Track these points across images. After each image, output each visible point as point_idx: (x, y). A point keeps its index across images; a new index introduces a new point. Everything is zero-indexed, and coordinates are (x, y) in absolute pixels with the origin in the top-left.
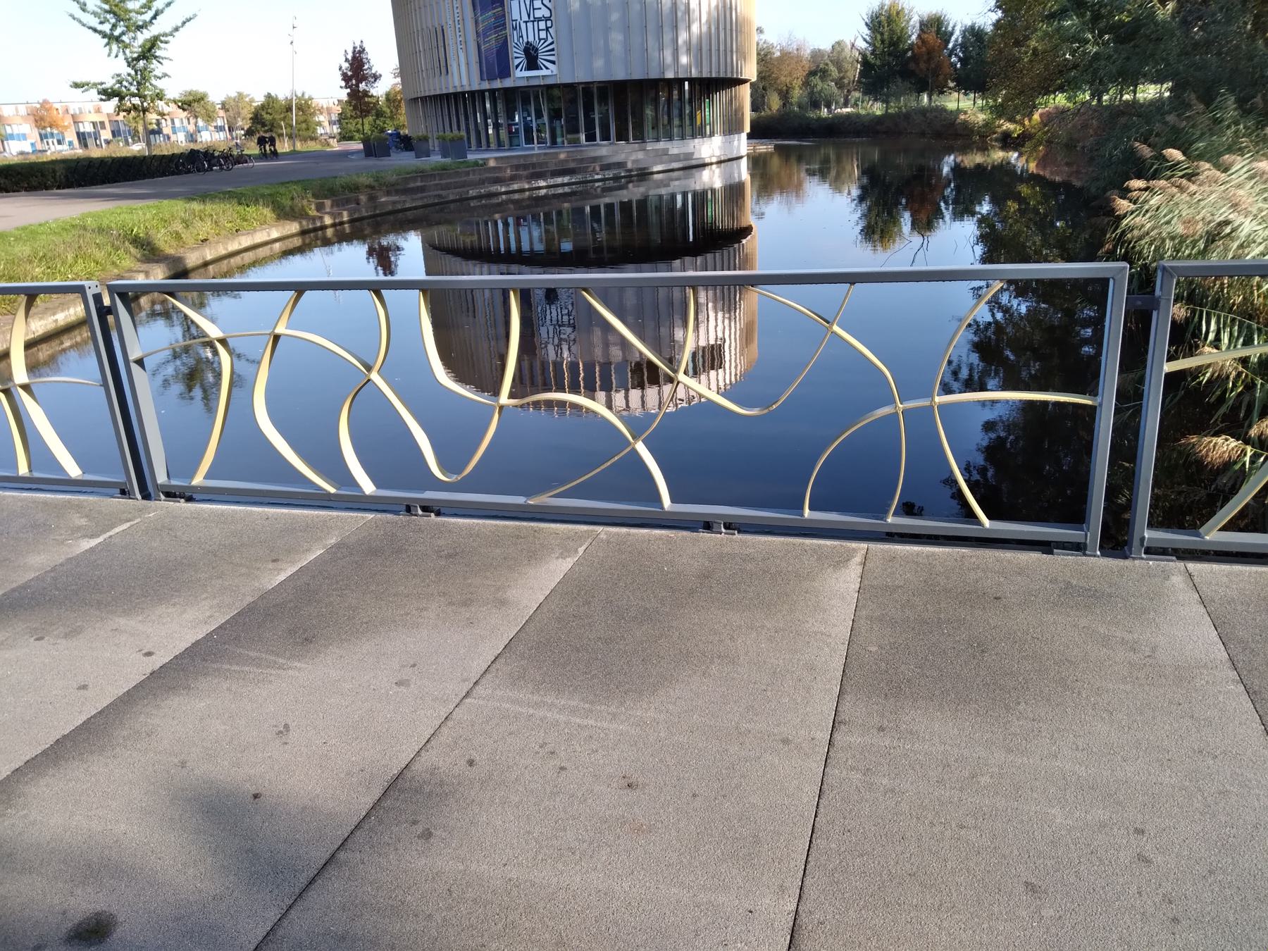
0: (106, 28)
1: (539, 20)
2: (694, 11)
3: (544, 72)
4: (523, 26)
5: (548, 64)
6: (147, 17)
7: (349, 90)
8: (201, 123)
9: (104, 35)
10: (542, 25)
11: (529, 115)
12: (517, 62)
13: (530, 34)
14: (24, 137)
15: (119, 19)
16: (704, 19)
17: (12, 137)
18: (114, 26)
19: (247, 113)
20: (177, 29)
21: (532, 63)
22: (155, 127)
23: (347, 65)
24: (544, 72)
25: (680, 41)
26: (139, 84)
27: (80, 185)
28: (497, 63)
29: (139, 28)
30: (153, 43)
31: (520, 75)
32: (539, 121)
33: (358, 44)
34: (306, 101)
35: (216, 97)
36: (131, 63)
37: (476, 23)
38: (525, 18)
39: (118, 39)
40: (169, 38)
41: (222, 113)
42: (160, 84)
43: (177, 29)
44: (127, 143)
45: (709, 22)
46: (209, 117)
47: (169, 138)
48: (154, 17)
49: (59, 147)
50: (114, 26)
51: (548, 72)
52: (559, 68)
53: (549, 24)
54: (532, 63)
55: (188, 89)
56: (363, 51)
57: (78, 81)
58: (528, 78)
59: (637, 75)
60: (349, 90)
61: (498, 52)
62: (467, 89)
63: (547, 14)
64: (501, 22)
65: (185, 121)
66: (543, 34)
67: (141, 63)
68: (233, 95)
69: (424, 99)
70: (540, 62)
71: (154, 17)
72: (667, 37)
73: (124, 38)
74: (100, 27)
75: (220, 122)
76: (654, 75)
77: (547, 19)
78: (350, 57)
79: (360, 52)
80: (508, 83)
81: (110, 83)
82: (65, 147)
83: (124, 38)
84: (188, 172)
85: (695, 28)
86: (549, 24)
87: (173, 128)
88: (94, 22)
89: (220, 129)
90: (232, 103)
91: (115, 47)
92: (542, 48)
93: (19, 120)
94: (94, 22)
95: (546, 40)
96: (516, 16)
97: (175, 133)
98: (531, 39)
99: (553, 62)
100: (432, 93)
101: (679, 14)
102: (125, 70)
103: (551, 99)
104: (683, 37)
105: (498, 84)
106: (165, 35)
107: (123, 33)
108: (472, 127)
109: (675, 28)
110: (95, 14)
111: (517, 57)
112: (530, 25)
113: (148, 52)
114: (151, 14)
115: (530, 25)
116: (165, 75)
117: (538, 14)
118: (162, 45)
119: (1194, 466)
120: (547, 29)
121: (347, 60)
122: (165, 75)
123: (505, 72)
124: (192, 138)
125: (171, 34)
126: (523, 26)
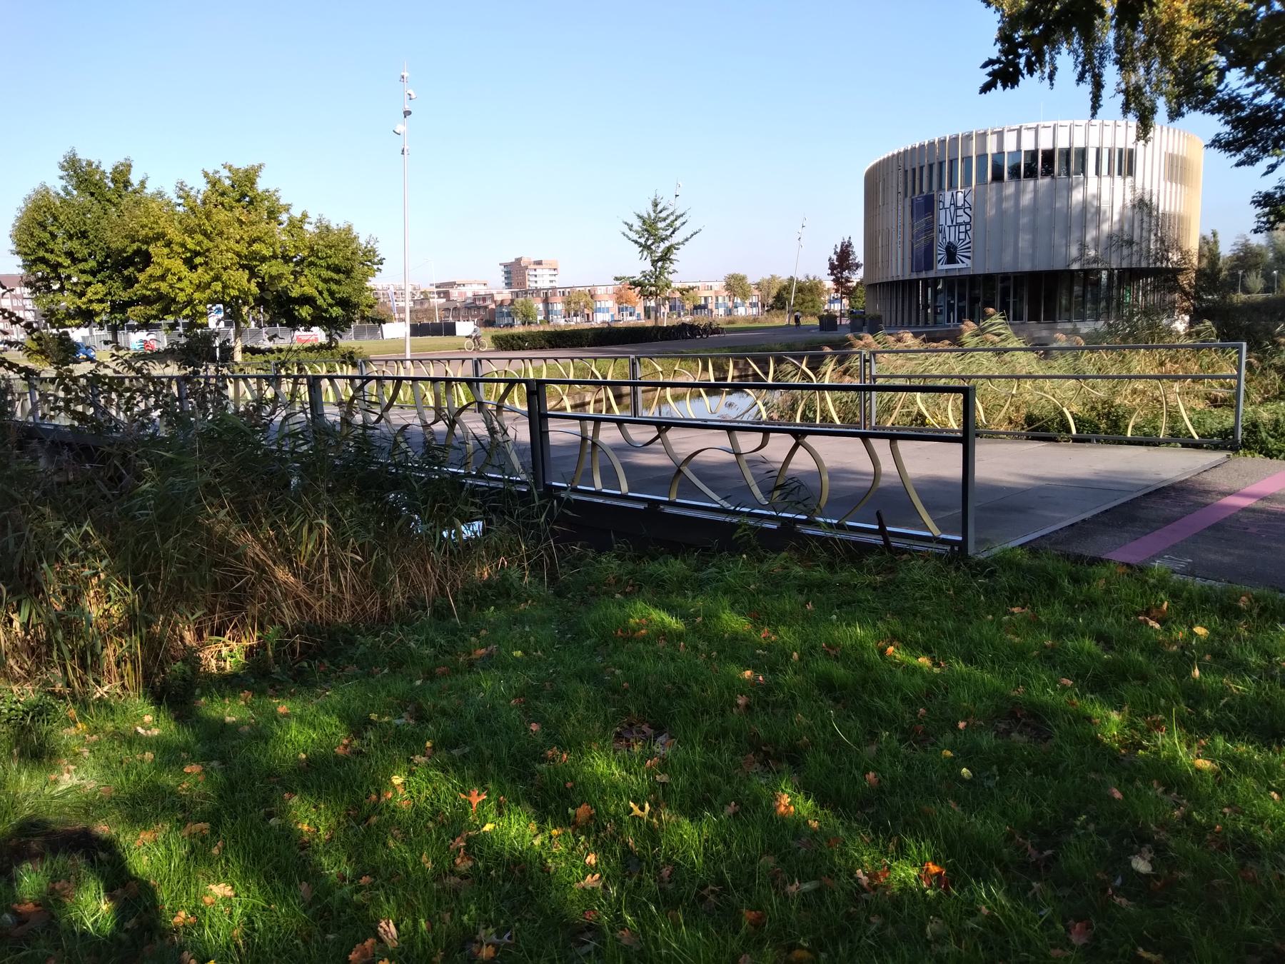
0: (642, 241)
1: (960, 224)
2: (1105, 212)
3: (960, 265)
4: (947, 229)
5: (963, 259)
6: (668, 233)
7: (833, 277)
8: (738, 300)
9: (641, 245)
10: (962, 228)
11: (953, 299)
12: (939, 257)
13: (951, 236)
14: (608, 310)
15: (650, 234)
16: (1116, 218)
17: (599, 310)
18: (648, 239)
19: (774, 292)
20: (687, 240)
21: (951, 258)
22: (703, 302)
23: (835, 257)
24: (960, 265)
25: (1088, 238)
26: (657, 277)
27: (601, 345)
28: (925, 259)
29: (663, 240)
30: (669, 249)
31: (942, 267)
32: (961, 304)
33: (846, 240)
34: (816, 284)
35: (752, 279)
36: (654, 263)
37: (913, 227)
38: (949, 223)
39: (649, 248)
40: (681, 246)
41: (756, 292)
42: (671, 277)
43: (687, 240)
44: (679, 315)
45: (1121, 220)
46: (745, 296)
47: (712, 312)
48: (673, 233)
49: (631, 318)
50: (648, 239)
51: (964, 265)
52: (973, 263)
53: (968, 227)
54: (951, 258)
55: (732, 272)
56: (850, 245)
57: (618, 276)
58: (947, 270)
59: (1042, 266)
60: (833, 277)
61: (926, 250)
62: (901, 278)
63: (967, 219)
64: (930, 228)
65: (727, 299)
66: (962, 236)
67: (660, 264)
68: (768, 277)
69: (882, 285)
70: (957, 258)
71: (673, 233)
72: (1075, 235)
73: (653, 247)
74: (639, 240)
75: (755, 300)
76: (1059, 266)
77: (966, 224)
78: (838, 250)
79: (847, 246)
80: (932, 274)
81: (638, 277)
82: (634, 318)
83: (653, 247)
84: (677, 339)
85: (1106, 227)
86: (968, 227)
87: (717, 304)
88: (636, 237)
89: (753, 305)
90: (766, 284)
91: (645, 253)
92: (960, 246)
93: (606, 297)
94: (636, 237)
95: (964, 240)
96: (942, 222)
97: (717, 308)
98: (952, 240)
99: (969, 258)
100: (885, 280)
101: (1089, 216)
102: (648, 266)
103: (972, 288)
104: (1091, 234)
105: (923, 275)
106: (678, 244)
107: (652, 244)
108: (914, 307)
109: (1084, 228)
110: (637, 232)
111: (940, 254)
112: (952, 229)
113: (665, 257)
114: (671, 230)
115: (952, 229)
116: (674, 271)
117: (960, 220)
118: (675, 251)
119: (126, 273)
120: (966, 232)
121: (836, 253)
122: (674, 271)
123: (929, 265)
124: (729, 312)
125: (683, 243)
126: (947, 229)
